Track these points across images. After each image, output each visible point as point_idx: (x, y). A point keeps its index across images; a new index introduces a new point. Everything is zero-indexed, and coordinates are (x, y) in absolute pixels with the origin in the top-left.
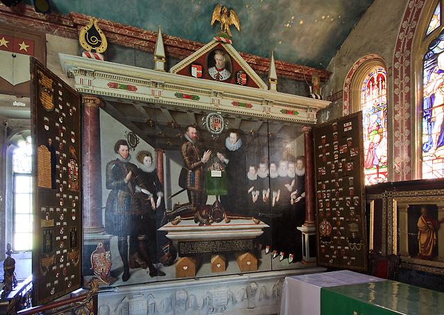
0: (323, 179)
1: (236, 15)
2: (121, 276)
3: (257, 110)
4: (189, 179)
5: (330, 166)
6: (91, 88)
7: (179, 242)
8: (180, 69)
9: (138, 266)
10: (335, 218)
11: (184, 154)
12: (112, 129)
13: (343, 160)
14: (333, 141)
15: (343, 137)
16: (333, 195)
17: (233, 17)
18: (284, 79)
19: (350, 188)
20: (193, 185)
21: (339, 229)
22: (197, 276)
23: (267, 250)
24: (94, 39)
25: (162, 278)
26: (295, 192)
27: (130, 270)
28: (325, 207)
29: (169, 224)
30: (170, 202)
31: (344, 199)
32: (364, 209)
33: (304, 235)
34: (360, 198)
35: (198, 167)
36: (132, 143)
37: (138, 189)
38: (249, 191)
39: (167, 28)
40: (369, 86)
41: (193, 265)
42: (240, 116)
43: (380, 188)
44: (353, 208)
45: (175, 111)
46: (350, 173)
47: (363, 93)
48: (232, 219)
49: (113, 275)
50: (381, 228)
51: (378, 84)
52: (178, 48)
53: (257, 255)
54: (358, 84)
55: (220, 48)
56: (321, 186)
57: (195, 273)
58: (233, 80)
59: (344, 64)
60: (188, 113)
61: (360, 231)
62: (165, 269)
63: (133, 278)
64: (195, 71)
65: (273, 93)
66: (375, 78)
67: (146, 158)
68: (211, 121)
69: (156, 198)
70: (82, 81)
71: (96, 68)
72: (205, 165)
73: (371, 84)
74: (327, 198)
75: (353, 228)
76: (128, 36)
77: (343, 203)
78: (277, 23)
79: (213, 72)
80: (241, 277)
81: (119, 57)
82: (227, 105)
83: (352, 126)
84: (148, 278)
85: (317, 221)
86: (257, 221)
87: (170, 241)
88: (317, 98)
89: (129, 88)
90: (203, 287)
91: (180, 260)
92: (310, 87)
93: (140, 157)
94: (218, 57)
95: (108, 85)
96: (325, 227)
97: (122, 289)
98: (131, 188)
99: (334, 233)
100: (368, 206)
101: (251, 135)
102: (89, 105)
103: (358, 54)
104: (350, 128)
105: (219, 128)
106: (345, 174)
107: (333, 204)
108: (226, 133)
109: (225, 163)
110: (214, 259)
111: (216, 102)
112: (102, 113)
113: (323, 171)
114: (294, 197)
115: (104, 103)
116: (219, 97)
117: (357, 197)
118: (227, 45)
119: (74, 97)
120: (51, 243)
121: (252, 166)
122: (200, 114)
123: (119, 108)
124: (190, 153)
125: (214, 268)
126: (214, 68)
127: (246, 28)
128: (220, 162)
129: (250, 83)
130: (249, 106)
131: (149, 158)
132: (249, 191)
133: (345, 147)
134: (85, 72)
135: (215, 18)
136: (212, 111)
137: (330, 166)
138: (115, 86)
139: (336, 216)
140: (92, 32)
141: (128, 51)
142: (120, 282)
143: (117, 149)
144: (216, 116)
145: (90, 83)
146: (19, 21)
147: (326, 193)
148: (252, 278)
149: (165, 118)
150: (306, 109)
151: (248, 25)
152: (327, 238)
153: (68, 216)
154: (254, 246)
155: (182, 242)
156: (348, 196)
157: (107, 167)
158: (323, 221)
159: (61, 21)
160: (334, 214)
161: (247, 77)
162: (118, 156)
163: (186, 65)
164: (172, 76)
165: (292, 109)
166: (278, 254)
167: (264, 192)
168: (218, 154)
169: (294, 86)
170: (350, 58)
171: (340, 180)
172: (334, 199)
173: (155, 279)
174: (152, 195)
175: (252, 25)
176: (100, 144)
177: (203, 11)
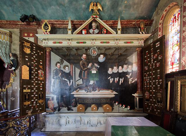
0: (146, 72)
1: (100, 4)
2: (57, 109)
3: (112, 44)
4: (83, 75)
5: (150, 65)
6: (47, 45)
7: (79, 99)
8: (78, 32)
9: (63, 106)
10: (151, 91)
11: (81, 65)
12: (55, 58)
13: (155, 62)
14: (153, 52)
15: (155, 50)
16: (150, 79)
17: (98, 5)
18: (128, 28)
19: (158, 76)
20: (84, 77)
21: (152, 96)
22: (86, 112)
23: (117, 104)
24: (46, 27)
25: (71, 111)
26: (132, 79)
27: (60, 108)
28: (147, 85)
29: (75, 92)
30: (75, 83)
31: (155, 81)
32: (164, 86)
33: (136, 98)
34: (163, 80)
35: (87, 70)
36: (61, 62)
37: (63, 79)
38: (109, 78)
39: (75, 17)
40: (173, 22)
41: (84, 108)
42: (105, 48)
43: (173, 74)
44: (159, 85)
45: (78, 49)
46: (158, 68)
47: (171, 26)
48: (100, 90)
49: (54, 109)
50: (173, 96)
51: (178, 19)
52: (79, 24)
53: (112, 105)
54: (167, 22)
55: (95, 21)
56: (146, 75)
57: (85, 110)
58: (100, 32)
59: (159, 13)
60: (83, 49)
61: (162, 97)
62: (73, 108)
63: (61, 111)
64: (84, 32)
65: (120, 35)
66: (177, 16)
67: (66, 67)
68: (92, 51)
69: (70, 82)
70: (44, 43)
71: (48, 37)
72: (89, 69)
73: (175, 20)
74: (148, 81)
75: (159, 95)
76: (61, 24)
77: (154, 83)
78: (120, 3)
79: (91, 31)
80: (104, 114)
81: (58, 32)
82: (98, 43)
83: (160, 44)
84: (67, 111)
85: (143, 91)
86: (112, 91)
87: (75, 98)
88: (145, 33)
89: (60, 43)
90: (87, 116)
91: (79, 105)
92: (139, 29)
93: (64, 67)
94: (94, 24)
95: (77, 43)
96: (147, 94)
97: (57, 114)
98: (61, 79)
99: (150, 98)
100: (167, 85)
101: (110, 55)
102: (48, 51)
103: (165, 6)
104: (159, 45)
105: (96, 53)
106: (156, 69)
107: (150, 84)
108: (99, 55)
109: (98, 67)
110: (92, 106)
111: (93, 43)
112: (52, 53)
113: (146, 68)
114: (131, 81)
115: (53, 49)
116: (118, 41)
117: (161, 80)
118: (97, 18)
119: (43, 49)
120: (29, 97)
121: (115, 66)
122: (88, 49)
123: (57, 50)
124: (83, 64)
125: (92, 109)
126: (92, 29)
127: (106, 9)
128: (96, 67)
129: (108, 32)
130: (108, 43)
131: (68, 67)
132: (109, 78)
133: (156, 55)
134: (45, 39)
135: (91, 8)
136: (92, 47)
137: (150, 65)
138: (55, 43)
139: (152, 89)
140: (46, 25)
141: (62, 29)
142: (57, 112)
143: (56, 65)
144: (94, 49)
145: (71, 43)
146: (30, 27)
147: (148, 78)
148: (108, 115)
149: (74, 52)
150: (138, 39)
151: (107, 7)
152: (148, 100)
153: (38, 89)
154: (110, 102)
155: (79, 98)
156: (157, 80)
157: (53, 71)
158: (146, 92)
159: (40, 24)
160: (151, 88)
161: (107, 30)
162: (57, 68)
163: (80, 30)
164: (75, 36)
165: (130, 41)
166: (122, 106)
167: (116, 79)
168: (95, 64)
169: (133, 30)
170: (162, 10)
171: (153, 72)
172: (151, 81)
173: (69, 111)
174: (68, 81)
175: (108, 7)
176: (51, 63)
177: (86, 6)
